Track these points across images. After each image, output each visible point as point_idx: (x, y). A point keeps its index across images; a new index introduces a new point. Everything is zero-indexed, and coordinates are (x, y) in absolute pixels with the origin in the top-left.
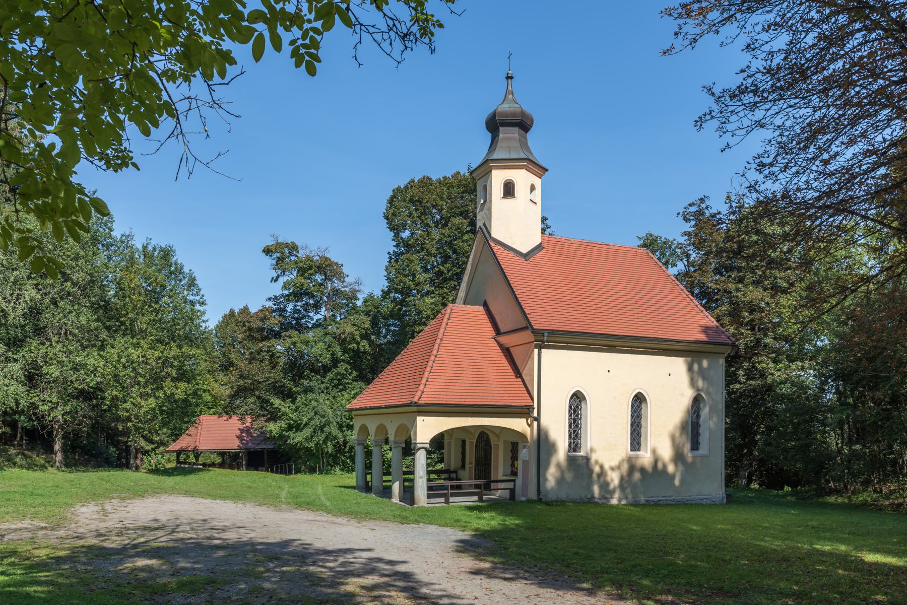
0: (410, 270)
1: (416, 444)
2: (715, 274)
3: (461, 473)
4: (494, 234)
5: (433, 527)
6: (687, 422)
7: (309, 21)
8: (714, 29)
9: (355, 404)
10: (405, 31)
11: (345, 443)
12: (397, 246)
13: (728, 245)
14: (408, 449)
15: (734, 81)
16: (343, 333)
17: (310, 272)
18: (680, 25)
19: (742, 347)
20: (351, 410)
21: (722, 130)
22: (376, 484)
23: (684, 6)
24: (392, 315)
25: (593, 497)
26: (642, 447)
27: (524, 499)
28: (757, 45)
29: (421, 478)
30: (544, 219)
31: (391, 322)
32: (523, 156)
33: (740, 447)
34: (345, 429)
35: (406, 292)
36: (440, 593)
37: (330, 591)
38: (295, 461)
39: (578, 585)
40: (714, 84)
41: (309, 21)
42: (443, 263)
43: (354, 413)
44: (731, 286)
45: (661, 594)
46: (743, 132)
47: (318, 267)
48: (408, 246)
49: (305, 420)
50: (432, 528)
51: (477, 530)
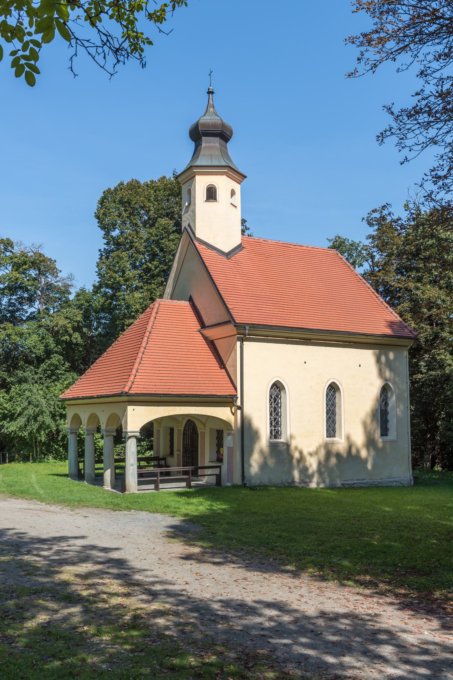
0: (119, 267)
1: (126, 432)
2: (397, 274)
3: (170, 460)
4: (199, 234)
5: (144, 513)
6: (377, 410)
7: (30, 34)
8: (391, 56)
9: (68, 394)
10: (117, 46)
11: (58, 431)
12: (108, 244)
13: (407, 248)
14: (119, 437)
15: (410, 103)
16: (56, 326)
17: (24, 267)
18: (362, 52)
19: (422, 340)
20: (63, 400)
21: (401, 145)
22: (88, 471)
23: (365, 35)
24: (103, 309)
25: (293, 482)
26: (337, 434)
27: (229, 484)
28: (429, 72)
29: (132, 465)
30: (243, 221)
31: (102, 315)
32: (224, 164)
33: (424, 432)
34: (58, 418)
35: (116, 287)
36: (152, 579)
37: (46, 580)
38: (9, 450)
39: (283, 568)
40: (393, 104)
41: (30, 34)
42: (151, 260)
43: (68, 402)
44: (411, 285)
45: (359, 574)
46: (419, 147)
47: (32, 263)
48: (118, 244)
49: (19, 409)
50: (143, 514)
51: (186, 515)
